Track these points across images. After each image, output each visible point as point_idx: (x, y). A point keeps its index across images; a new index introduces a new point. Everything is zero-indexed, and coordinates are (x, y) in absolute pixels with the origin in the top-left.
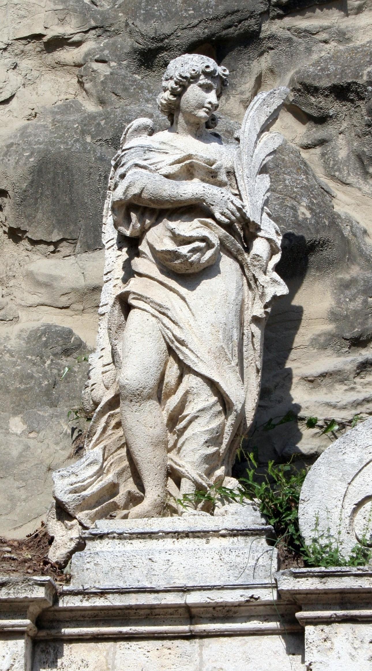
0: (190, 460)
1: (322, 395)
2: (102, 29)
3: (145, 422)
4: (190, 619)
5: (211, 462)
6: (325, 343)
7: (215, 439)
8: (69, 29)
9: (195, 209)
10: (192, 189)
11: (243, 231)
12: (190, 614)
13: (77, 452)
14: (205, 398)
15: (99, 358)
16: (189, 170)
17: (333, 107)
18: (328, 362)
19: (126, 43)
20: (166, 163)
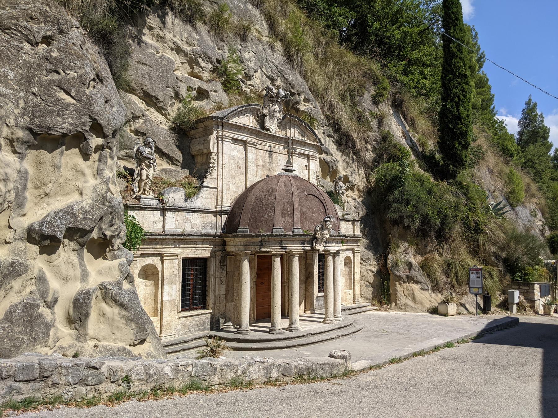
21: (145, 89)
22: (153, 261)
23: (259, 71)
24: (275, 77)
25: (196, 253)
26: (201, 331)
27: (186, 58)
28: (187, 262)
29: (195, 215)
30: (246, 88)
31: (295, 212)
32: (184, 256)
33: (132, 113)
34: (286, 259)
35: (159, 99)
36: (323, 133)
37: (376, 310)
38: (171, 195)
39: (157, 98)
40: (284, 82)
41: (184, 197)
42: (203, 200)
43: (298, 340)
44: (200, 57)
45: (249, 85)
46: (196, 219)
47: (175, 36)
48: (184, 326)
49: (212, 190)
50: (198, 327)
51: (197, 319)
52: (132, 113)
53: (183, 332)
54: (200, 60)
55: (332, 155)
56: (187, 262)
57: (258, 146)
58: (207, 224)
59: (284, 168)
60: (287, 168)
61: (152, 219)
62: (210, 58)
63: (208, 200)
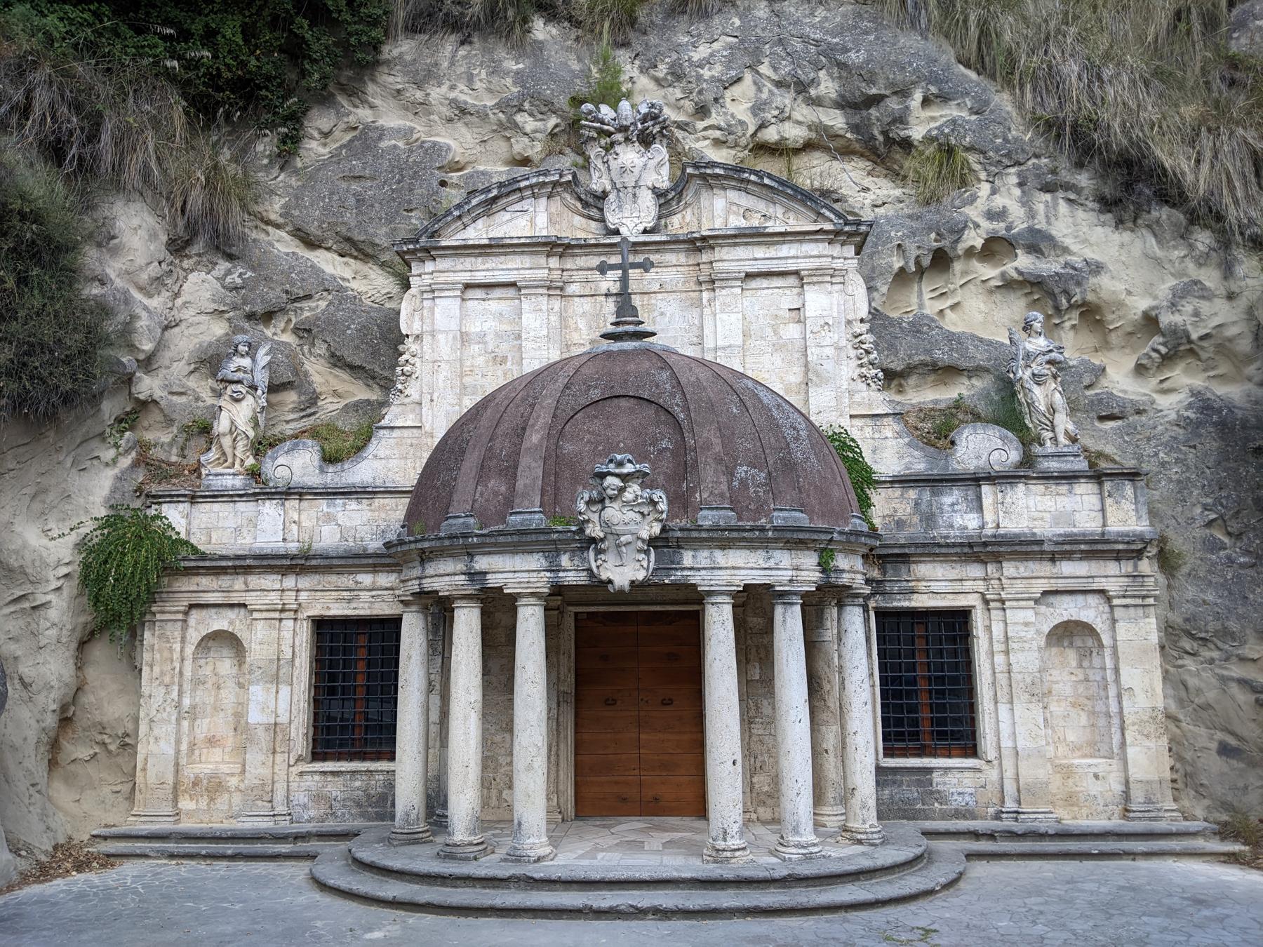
6: (293, 411)
10: (240, 375)
21: (343, 230)
22: (231, 623)
23: (748, 77)
24: (806, 74)
25: (354, 605)
26: (370, 820)
27: (487, 128)
28: (327, 631)
29: (353, 505)
30: (698, 140)
31: (525, 461)
32: (317, 611)
33: (287, 292)
34: (498, 611)
35: (377, 245)
36: (1020, 185)
37: (1232, 859)
38: (280, 461)
39: (374, 245)
40: (840, 78)
41: (317, 462)
42: (378, 464)
43: (691, 905)
44: (520, 110)
45: (706, 129)
46: (354, 515)
47: (452, 88)
48: (318, 797)
49: (406, 433)
50: (359, 805)
51: (358, 784)
52: (287, 292)
53: (313, 813)
54: (519, 118)
55: (1066, 250)
56: (327, 631)
57: (572, 289)
58: (363, 524)
59: (611, 329)
60: (621, 329)
61: (231, 522)
62: (548, 103)
63: (393, 463)
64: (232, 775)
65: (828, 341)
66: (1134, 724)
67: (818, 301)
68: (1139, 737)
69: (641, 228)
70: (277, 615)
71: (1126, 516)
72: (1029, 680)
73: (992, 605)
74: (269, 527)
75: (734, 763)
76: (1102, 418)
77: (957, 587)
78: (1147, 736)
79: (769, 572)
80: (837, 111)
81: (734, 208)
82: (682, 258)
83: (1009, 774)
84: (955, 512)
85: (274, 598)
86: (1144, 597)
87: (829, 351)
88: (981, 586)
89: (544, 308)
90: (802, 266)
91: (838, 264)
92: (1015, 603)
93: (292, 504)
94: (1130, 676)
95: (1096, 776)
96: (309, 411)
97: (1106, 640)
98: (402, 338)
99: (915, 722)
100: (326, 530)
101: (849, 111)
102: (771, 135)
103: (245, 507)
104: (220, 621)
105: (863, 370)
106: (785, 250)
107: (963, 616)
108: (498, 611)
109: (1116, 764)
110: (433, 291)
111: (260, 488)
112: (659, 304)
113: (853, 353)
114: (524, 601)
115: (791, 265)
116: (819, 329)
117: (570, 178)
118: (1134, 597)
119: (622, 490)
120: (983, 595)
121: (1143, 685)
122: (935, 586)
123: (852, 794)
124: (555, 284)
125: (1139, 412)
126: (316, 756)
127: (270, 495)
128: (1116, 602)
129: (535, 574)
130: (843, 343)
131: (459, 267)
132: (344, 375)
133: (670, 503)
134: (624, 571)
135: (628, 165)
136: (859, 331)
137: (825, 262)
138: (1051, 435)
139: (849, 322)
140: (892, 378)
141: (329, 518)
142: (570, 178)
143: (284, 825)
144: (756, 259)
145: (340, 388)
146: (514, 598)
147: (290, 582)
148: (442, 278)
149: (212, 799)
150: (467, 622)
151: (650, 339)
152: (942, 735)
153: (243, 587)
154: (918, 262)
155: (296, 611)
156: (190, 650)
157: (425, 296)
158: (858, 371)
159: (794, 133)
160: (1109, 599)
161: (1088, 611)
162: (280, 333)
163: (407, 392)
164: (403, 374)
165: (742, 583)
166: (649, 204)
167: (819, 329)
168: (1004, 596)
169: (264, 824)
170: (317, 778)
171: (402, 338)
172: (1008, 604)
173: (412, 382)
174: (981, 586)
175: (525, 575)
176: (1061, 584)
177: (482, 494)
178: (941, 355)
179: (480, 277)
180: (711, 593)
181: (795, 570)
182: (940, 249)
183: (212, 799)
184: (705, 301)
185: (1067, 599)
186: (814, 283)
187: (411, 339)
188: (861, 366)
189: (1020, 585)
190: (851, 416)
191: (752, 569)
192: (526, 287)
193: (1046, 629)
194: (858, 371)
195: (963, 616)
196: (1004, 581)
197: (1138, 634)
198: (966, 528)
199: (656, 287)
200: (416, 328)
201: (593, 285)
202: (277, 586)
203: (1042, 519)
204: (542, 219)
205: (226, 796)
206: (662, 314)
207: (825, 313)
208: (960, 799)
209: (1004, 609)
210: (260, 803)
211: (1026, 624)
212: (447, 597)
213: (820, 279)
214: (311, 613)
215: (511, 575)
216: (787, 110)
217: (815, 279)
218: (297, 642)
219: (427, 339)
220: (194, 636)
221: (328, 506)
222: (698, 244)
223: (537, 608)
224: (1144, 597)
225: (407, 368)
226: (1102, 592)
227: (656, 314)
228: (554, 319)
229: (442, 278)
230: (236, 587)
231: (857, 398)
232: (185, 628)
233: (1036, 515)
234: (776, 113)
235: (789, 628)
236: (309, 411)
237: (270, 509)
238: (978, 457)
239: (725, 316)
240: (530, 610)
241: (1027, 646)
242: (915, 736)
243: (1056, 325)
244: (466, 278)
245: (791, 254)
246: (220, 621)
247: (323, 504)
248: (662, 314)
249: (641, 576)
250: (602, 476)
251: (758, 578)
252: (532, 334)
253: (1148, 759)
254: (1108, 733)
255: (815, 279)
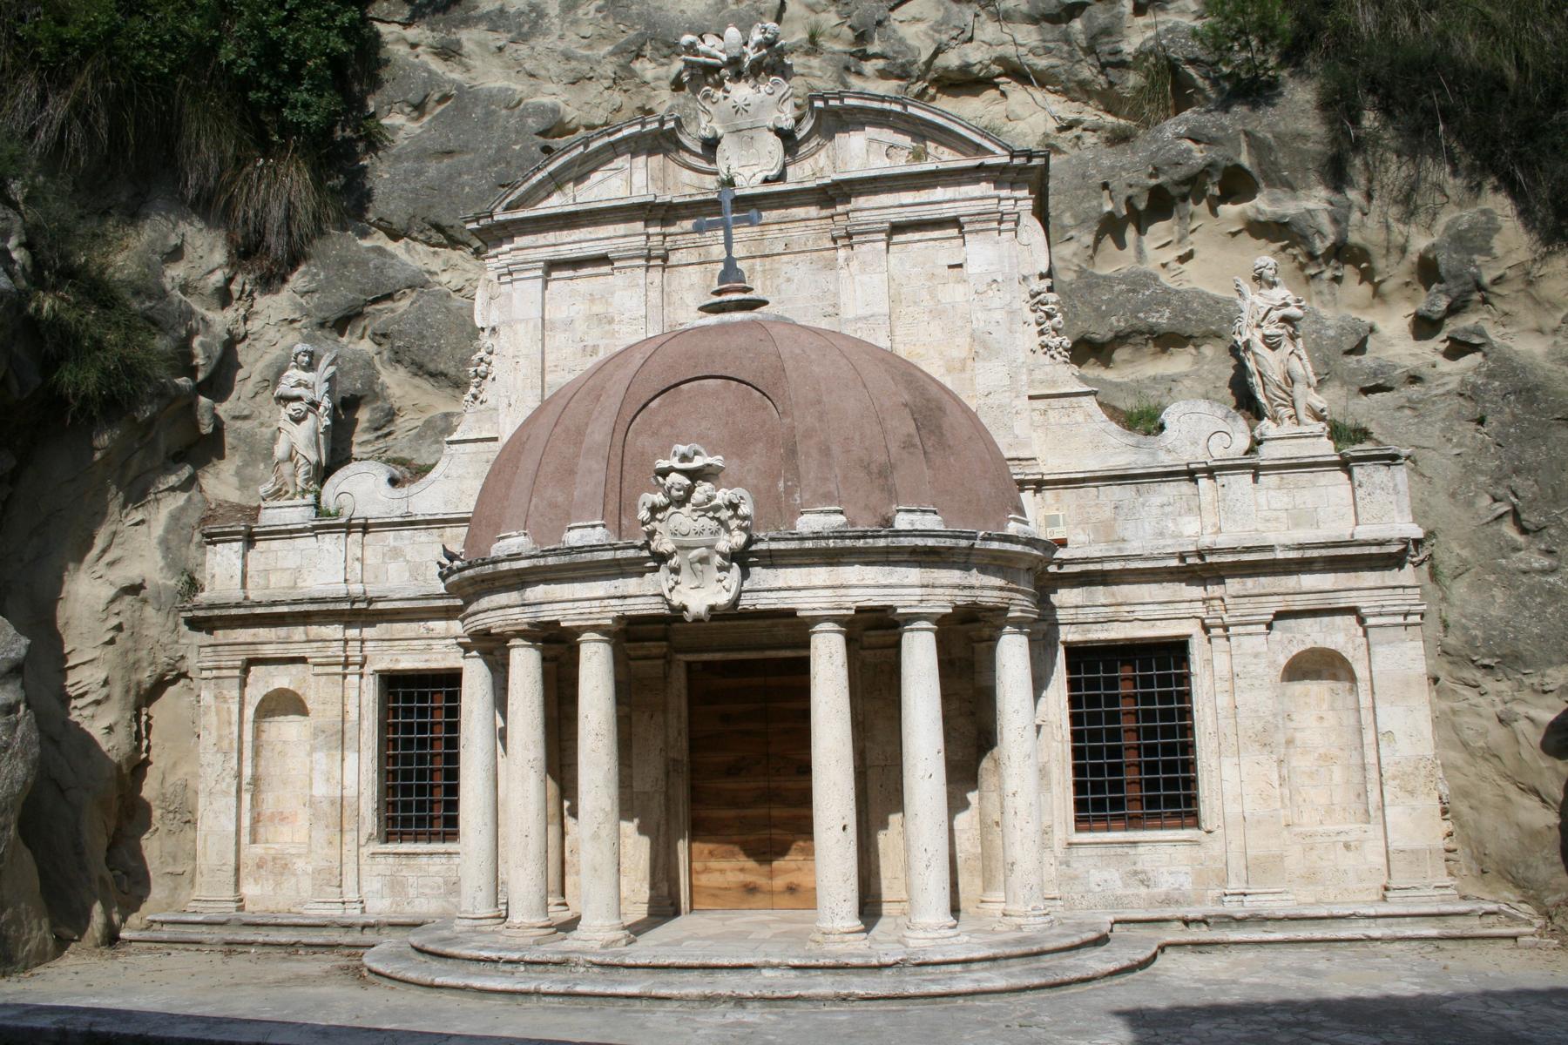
0: (300, 481)
1: (363, 449)
2: (308, 315)
3: (287, 468)
4: (290, 533)
5: (307, 481)
6: (366, 430)
7: (307, 473)
8: (296, 316)
9: (298, 398)
10: (297, 392)
11: (314, 405)
12: (291, 532)
13: (1220, 337)
14: (302, 461)
15: (950, 267)
16: (299, 384)
17: (383, 341)
18: (366, 437)
19: (315, 320)
20: (292, 381)
32: (385, 664)
34: (557, 646)
56: (395, 684)
57: (674, 258)
64: (299, 856)
65: (997, 303)
66: (1394, 778)
67: (981, 253)
68: (1400, 794)
69: (760, 177)
70: (339, 669)
71: (1383, 509)
72: (1259, 726)
73: (1214, 632)
74: (320, 567)
75: (844, 828)
76: (1366, 391)
77: (1169, 611)
78: (1412, 793)
79: (890, 591)
80: (1031, 27)
81: (875, 145)
82: (813, 211)
83: (1235, 847)
84: (1167, 515)
85: (336, 649)
86: (1406, 615)
87: (998, 315)
88: (1199, 609)
89: (642, 282)
90: (961, 211)
91: (1007, 206)
92: (1241, 629)
93: (356, 537)
94: (1389, 716)
95: (1347, 846)
96: (386, 430)
97: (1360, 670)
98: (476, 332)
99: (1117, 786)
100: (393, 567)
101: (1045, 25)
102: (951, 59)
103: (306, 543)
104: (282, 678)
105: (1044, 338)
106: (939, 193)
107: (1177, 650)
108: (557, 646)
109: (1375, 830)
110: (510, 273)
111: (327, 523)
112: (785, 268)
113: (1032, 317)
114: (585, 636)
115: (948, 211)
116: (984, 288)
117: (672, 124)
118: (1394, 614)
119: (689, 491)
120: (1202, 620)
121: (1407, 723)
122: (1140, 612)
123: (1012, 870)
124: (654, 253)
125: (1415, 379)
126: (388, 837)
127: (329, 528)
128: (1370, 621)
129: (597, 603)
130: (1017, 305)
131: (541, 242)
132: (425, 384)
133: (756, 504)
134: (700, 594)
135: (740, 103)
136: (1036, 289)
137: (991, 205)
138: (1292, 412)
139: (1025, 278)
140: (1086, 350)
141: (396, 553)
142: (672, 124)
143: (353, 913)
144: (902, 206)
145: (423, 401)
146: (576, 632)
147: (353, 633)
148: (521, 256)
149: (278, 884)
150: (525, 663)
151: (764, 309)
152: (1152, 802)
153: (303, 638)
154: (1129, 201)
155: (362, 666)
156: (249, 712)
157: (503, 279)
158: (1039, 340)
159: (976, 55)
160: (1361, 621)
161: (1336, 635)
162: (359, 345)
163: (481, 397)
164: (477, 375)
165: (854, 606)
166: (771, 148)
167: (984, 288)
168: (1227, 620)
169: (335, 912)
170: (391, 860)
171: (476, 332)
172: (1232, 629)
173: (487, 384)
174: (1199, 609)
175: (586, 604)
176: (1299, 603)
177: (536, 507)
178: (1162, 318)
179: (567, 252)
180: (817, 620)
181: (942, 589)
182: (1159, 187)
183: (278, 884)
184: (841, 261)
185: (1307, 622)
186: (977, 232)
187: (487, 333)
188: (1042, 333)
189: (1247, 606)
190: (1030, 397)
191: (868, 587)
192: (619, 259)
193: (1283, 661)
194: (1039, 340)
195: (1177, 650)
196: (1227, 600)
197: (1398, 662)
198: (1181, 536)
199: (780, 248)
200: (494, 318)
201: (702, 250)
202: (340, 636)
203: (1277, 519)
204: (639, 178)
205: (293, 880)
206: (789, 280)
207: (992, 268)
208: (1172, 880)
209: (1228, 638)
210: (329, 889)
211: (1256, 656)
212: (501, 634)
213: (985, 226)
214: (378, 667)
215: (569, 605)
216: (969, 29)
217: (978, 226)
218: (364, 698)
219: (503, 331)
220: (255, 694)
221: (395, 539)
222: (832, 195)
223: (602, 645)
224: (1406, 615)
225: (483, 367)
226: (1352, 611)
227: (781, 280)
228: (654, 295)
229: (521, 256)
230: (296, 638)
231: (1038, 375)
232: (243, 684)
233: (1269, 514)
234: (954, 33)
235: (920, 657)
236: (386, 430)
237: (330, 544)
238: (1195, 443)
239: (865, 278)
240: (593, 647)
241: (1257, 683)
242: (1118, 804)
243: (1313, 277)
244: (548, 254)
245: (947, 198)
246: (282, 678)
247: (390, 537)
248: (789, 280)
249: (723, 599)
250: (665, 473)
251: (876, 599)
252: (627, 315)
253: (1415, 823)
254: (1368, 791)
255: (978, 226)
